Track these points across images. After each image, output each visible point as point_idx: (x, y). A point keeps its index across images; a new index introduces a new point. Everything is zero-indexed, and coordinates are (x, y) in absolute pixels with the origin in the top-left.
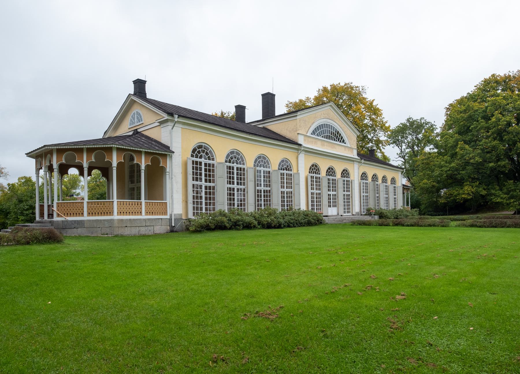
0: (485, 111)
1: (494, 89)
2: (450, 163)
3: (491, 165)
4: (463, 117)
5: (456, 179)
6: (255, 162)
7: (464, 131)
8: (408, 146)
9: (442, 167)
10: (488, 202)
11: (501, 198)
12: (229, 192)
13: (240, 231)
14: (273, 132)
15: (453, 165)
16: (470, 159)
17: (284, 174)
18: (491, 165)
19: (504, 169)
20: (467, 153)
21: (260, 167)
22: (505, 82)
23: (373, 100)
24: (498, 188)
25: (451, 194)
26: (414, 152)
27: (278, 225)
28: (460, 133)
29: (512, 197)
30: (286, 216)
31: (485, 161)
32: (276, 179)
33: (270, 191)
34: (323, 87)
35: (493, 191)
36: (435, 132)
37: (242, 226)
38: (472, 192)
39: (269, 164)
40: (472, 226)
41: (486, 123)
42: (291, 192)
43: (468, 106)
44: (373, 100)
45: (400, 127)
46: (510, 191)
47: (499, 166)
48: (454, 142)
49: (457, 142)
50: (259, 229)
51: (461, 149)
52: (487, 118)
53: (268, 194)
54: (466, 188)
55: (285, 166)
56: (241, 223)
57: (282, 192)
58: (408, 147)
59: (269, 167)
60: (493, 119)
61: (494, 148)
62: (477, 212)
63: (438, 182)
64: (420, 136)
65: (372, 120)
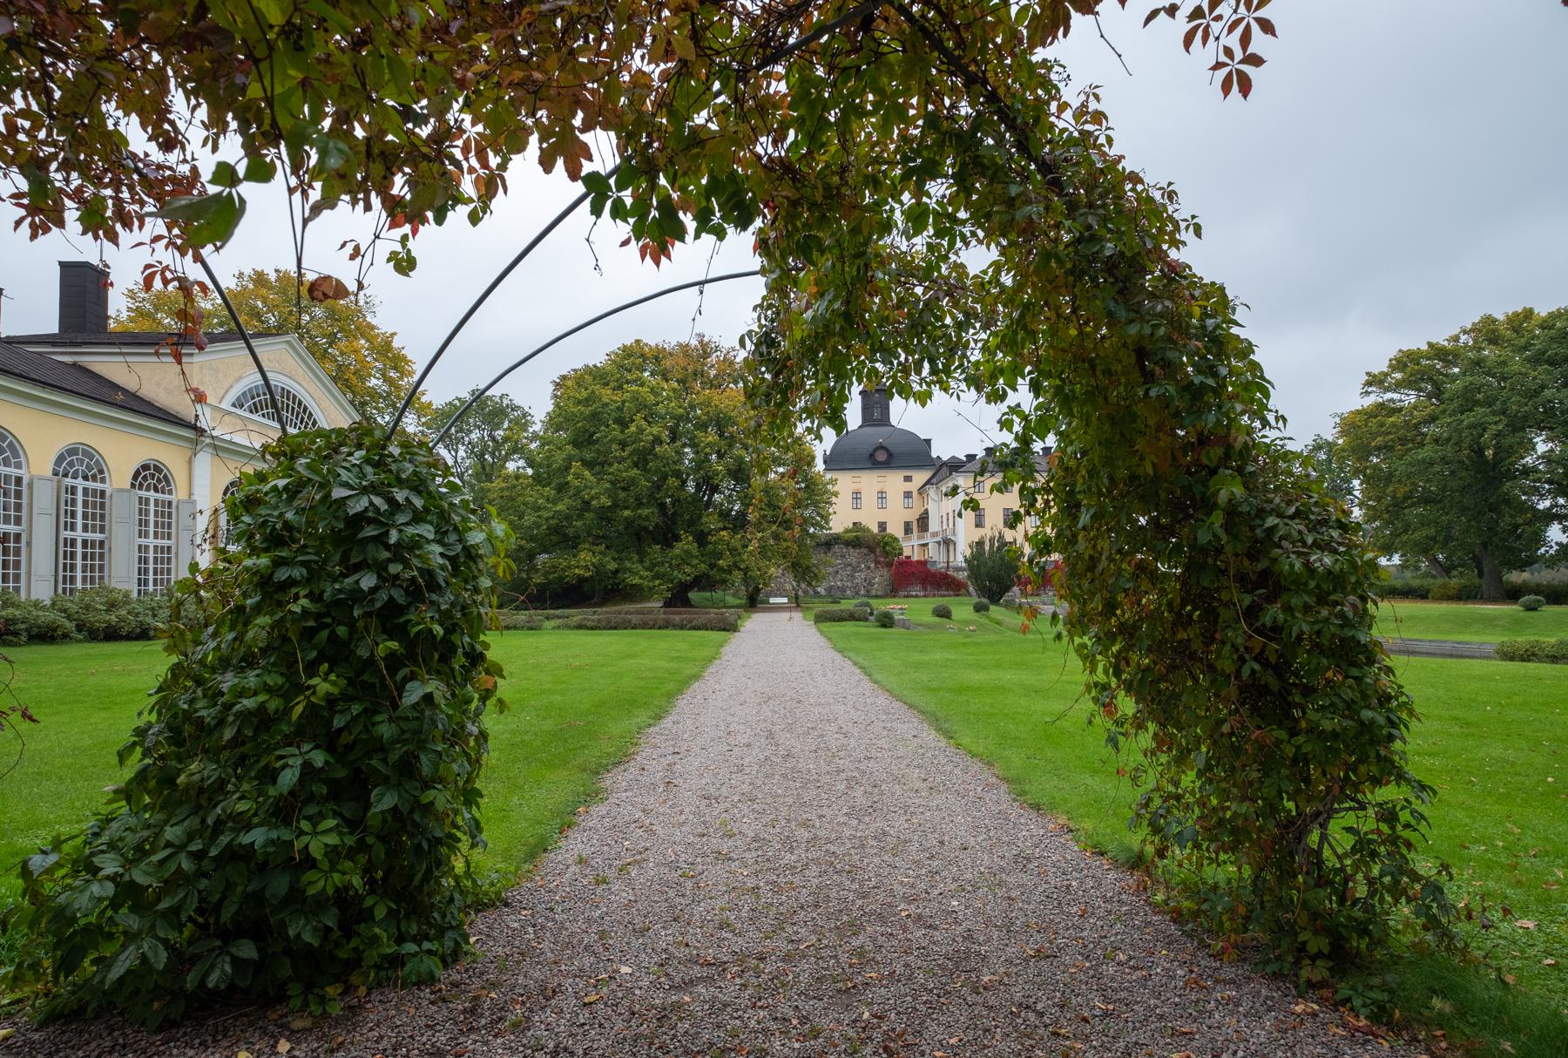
0: (620, 409)
1: (638, 369)
2: (555, 503)
3: (627, 513)
4: (582, 413)
5: (565, 535)
6: (135, 477)
7: (583, 440)
8: (472, 452)
9: (539, 509)
10: (619, 584)
11: (641, 577)
12: (151, 541)
13: (22, 649)
14: (111, 382)
15: (560, 507)
16: (592, 498)
17: (147, 500)
18: (627, 513)
19: (647, 523)
20: (586, 487)
21: (148, 489)
22: (656, 358)
23: (393, 335)
24: (636, 557)
25: (554, 567)
26: (483, 467)
27: (138, 630)
28: (576, 443)
29: (657, 576)
30: (160, 608)
31: (615, 505)
32: (122, 514)
33: (102, 543)
34: (256, 272)
35: (628, 564)
36: (531, 430)
37: (25, 634)
38: (593, 564)
39: (16, 455)
40: (580, 627)
41: (622, 432)
42: (169, 548)
43: (593, 392)
44: (393, 335)
45: (455, 406)
46: (655, 565)
47: (640, 517)
48: (564, 460)
49: (569, 460)
50: (80, 641)
51: (577, 476)
52: (623, 423)
53: (97, 553)
54: (582, 555)
55: (150, 475)
56: (23, 626)
57: (140, 546)
58: (471, 453)
59: (170, 492)
60: (633, 429)
61: (633, 482)
62: (603, 603)
63: (532, 539)
64: (499, 434)
65: (387, 379)
